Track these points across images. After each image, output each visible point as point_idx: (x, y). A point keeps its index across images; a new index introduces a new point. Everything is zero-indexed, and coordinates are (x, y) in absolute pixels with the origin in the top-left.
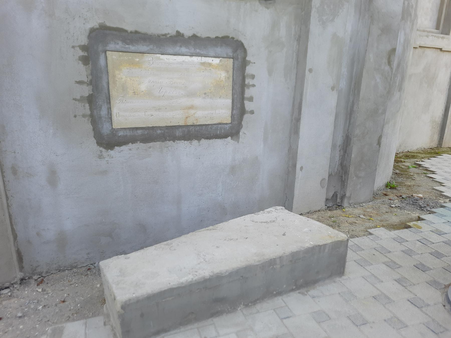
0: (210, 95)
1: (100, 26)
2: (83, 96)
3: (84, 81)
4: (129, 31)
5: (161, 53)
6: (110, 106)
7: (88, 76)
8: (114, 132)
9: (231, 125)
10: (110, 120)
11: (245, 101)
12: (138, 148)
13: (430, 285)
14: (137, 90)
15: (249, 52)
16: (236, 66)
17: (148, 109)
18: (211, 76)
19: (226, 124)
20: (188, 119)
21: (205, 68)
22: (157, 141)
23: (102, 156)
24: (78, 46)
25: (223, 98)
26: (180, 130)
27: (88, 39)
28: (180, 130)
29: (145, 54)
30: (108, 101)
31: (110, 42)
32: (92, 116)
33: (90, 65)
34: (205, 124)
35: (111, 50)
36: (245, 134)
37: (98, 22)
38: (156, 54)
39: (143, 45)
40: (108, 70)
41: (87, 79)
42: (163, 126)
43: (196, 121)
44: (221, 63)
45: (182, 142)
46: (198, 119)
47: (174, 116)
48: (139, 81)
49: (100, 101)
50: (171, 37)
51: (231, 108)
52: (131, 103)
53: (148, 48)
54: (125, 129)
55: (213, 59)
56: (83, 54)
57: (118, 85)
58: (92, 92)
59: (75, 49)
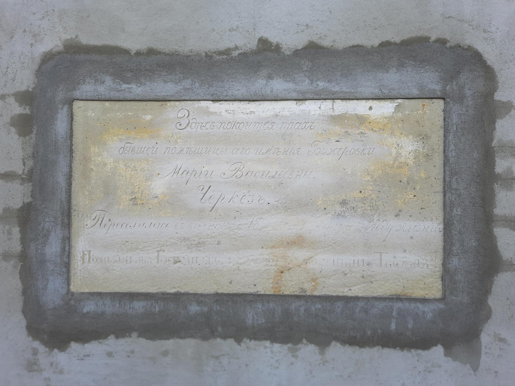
0: (362, 207)
1: (65, 46)
2: (9, 208)
3: (15, 172)
4: (133, 52)
5: (211, 98)
6: (69, 233)
7: (25, 161)
8: (72, 302)
9: (442, 306)
10: (64, 270)
11: (495, 230)
12: (132, 352)
13: (202, 199)
14: (142, 194)
15: (502, 77)
16: (455, 119)
17: (168, 243)
18: (366, 152)
19: (424, 301)
20: (286, 276)
21: (344, 130)
22: (189, 337)
23: (35, 364)
24: (13, 95)
25: (411, 216)
26: (260, 307)
27: (37, 77)
28: (258, 308)
29: (168, 104)
30: (66, 221)
31: (84, 81)
32: (23, 257)
33: (33, 136)
34: (345, 294)
35: (84, 98)
36: (502, 340)
37: (62, 39)
38: (198, 102)
39: (165, 82)
40: (72, 145)
41: (22, 167)
42: (206, 292)
43: (313, 284)
44: (400, 114)
45: (266, 347)
46: (317, 278)
47: (240, 264)
48: (148, 170)
49: (46, 220)
50: (244, 55)
51: (441, 251)
52: (124, 226)
53: (179, 87)
54: (100, 294)
55: (370, 103)
56: (22, 112)
57: (93, 181)
58: (30, 200)
59: (5, 102)
